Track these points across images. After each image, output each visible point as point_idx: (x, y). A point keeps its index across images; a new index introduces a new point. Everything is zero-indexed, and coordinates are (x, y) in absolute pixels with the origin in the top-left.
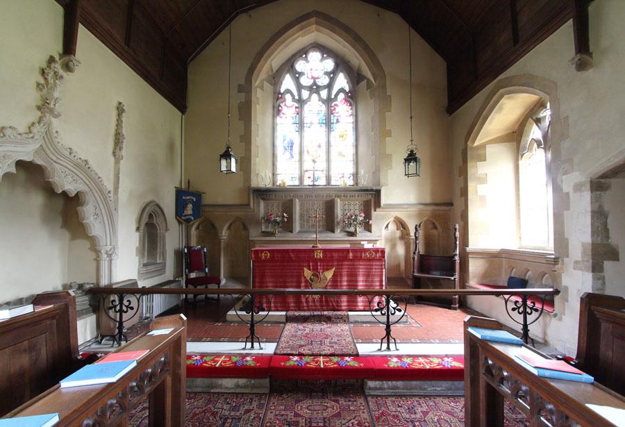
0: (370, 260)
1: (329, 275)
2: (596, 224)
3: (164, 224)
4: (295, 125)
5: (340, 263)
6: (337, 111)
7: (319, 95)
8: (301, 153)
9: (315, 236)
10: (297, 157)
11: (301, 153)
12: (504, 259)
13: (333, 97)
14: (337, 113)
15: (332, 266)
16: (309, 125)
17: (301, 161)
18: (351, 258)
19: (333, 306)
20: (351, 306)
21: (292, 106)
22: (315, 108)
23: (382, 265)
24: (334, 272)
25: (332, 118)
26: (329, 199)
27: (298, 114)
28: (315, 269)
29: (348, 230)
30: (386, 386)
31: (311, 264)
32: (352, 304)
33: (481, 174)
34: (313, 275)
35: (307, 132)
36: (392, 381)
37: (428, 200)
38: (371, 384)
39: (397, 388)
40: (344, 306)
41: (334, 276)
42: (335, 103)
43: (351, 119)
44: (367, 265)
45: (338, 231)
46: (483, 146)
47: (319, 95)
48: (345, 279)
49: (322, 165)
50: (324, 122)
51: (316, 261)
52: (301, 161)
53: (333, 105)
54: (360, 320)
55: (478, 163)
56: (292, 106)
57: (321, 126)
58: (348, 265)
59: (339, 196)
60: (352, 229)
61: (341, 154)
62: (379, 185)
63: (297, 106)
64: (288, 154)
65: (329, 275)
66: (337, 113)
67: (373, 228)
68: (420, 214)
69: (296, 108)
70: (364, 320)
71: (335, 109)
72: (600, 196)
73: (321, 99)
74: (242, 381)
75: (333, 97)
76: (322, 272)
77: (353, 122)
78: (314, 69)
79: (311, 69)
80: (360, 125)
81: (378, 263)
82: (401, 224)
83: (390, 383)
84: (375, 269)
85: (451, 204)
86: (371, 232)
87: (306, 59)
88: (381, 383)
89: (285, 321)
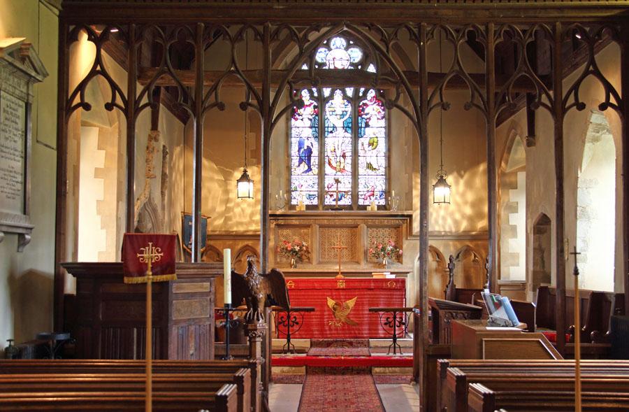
0: (390, 289)
1: (351, 303)
2: (536, 258)
3: (529, 232)
4: (314, 129)
6: (366, 111)
7: (344, 92)
8: (321, 166)
9: (338, 267)
10: (315, 170)
11: (321, 166)
13: (361, 94)
14: (366, 114)
15: (355, 296)
16: (330, 129)
17: (321, 175)
19: (355, 333)
20: (372, 334)
21: (310, 105)
22: (338, 105)
23: (402, 295)
25: (360, 121)
27: (317, 115)
30: (387, 371)
32: (373, 332)
33: (513, 203)
34: (336, 304)
35: (330, 141)
36: (391, 367)
38: (377, 370)
39: (395, 372)
40: (366, 334)
41: (356, 304)
42: (364, 102)
43: (383, 123)
44: (388, 295)
47: (344, 92)
49: (346, 185)
50: (350, 125)
52: (321, 175)
53: (361, 104)
54: (379, 345)
55: (510, 190)
56: (310, 105)
57: (346, 131)
61: (370, 166)
62: (412, 210)
63: (316, 104)
64: (304, 167)
65: (351, 303)
66: (366, 114)
67: (404, 260)
69: (315, 107)
70: (384, 345)
71: (363, 110)
72: (539, 238)
73: (345, 97)
74: (286, 369)
75: (361, 94)
77: (385, 127)
78: (337, 58)
79: (334, 59)
80: (394, 132)
81: (398, 293)
83: (390, 369)
84: (396, 298)
87: (328, 46)
88: (384, 369)
89: (309, 346)
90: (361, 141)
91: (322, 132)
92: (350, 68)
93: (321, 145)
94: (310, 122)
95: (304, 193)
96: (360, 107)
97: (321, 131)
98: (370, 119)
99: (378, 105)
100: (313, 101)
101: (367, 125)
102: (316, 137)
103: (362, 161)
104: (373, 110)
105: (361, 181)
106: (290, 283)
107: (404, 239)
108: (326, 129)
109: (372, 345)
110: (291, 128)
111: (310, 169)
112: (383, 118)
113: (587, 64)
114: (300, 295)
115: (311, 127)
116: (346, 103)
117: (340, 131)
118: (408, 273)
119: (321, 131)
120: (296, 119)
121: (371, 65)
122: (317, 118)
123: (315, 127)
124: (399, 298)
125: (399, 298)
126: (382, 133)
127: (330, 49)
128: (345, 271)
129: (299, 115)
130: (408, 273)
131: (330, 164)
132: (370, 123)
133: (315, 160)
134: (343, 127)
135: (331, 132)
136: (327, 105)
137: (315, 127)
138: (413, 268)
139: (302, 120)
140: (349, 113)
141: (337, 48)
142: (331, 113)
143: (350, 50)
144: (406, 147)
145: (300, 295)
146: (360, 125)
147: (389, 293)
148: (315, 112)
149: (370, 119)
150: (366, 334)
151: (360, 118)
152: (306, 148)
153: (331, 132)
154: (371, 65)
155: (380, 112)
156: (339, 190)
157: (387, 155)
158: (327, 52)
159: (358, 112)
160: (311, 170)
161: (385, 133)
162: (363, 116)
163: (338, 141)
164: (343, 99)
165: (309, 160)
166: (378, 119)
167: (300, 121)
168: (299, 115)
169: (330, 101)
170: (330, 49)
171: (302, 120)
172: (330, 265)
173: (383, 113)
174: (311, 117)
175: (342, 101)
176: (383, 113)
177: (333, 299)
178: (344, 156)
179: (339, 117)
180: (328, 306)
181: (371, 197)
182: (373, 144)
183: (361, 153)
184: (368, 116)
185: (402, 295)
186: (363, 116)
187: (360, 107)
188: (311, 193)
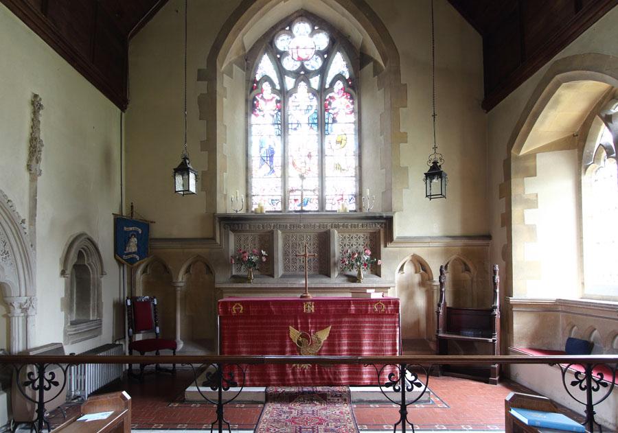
0: (378, 315)
4: (276, 126)
5: (339, 320)
8: (284, 166)
10: (278, 172)
11: (284, 166)
12: (561, 314)
13: (327, 86)
15: (328, 324)
18: (353, 312)
19: (329, 379)
21: (272, 100)
23: (395, 323)
24: (330, 332)
25: (326, 116)
26: (323, 230)
27: (279, 110)
28: (305, 328)
29: (349, 273)
31: (299, 321)
35: (292, 136)
37: (457, 231)
41: (331, 337)
42: (331, 95)
45: (335, 274)
46: (532, 156)
47: (308, 84)
48: (345, 341)
49: (312, 182)
50: (316, 121)
51: (305, 316)
54: (365, 399)
56: (272, 100)
58: (348, 322)
59: (337, 227)
60: (354, 272)
61: (338, 167)
63: (279, 99)
64: (266, 168)
65: (324, 335)
66: (333, 109)
67: (383, 271)
68: (447, 251)
69: (278, 102)
70: (371, 399)
71: (330, 104)
73: (311, 90)
75: (327, 86)
76: (315, 333)
77: (354, 123)
79: (297, 48)
81: (389, 320)
82: (420, 265)
84: (386, 327)
85: (488, 237)
86: (379, 276)
87: (290, 33)
90: (327, 139)
91: (284, 130)
92: (318, 403)
93: (284, 142)
94: (271, 118)
95: (266, 198)
96: (326, 100)
97: (284, 126)
98: (337, 113)
99: (347, 98)
100: (275, 95)
101: (334, 121)
102: (279, 135)
103: (329, 162)
104: (341, 104)
105: (328, 183)
106: (237, 306)
107: (382, 246)
108: (290, 126)
109: (354, 398)
110: (251, 125)
111: (272, 170)
112: (353, 111)
113: (112, 415)
114: (251, 324)
115: (274, 124)
116: (312, 97)
117: (305, 128)
118: (389, 288)
119: (284, 126)
120: (257, 115)
121: (338, 53)
122: (279, 113)
123: (278, 124)
124: (390, 327)
125: (391, 331)
126: (352, 129)
127: (293, 37)
128: (313, 286)
129: (260, 110)
130: (389, 288)
131: (294, 164)
132: (337, 119)
133: (278, 160)
134: (309, 124)
135: (295, 129)
136: (291, 99)
137: (278, 124)
138: (393, 282)
139: (263, 116)
140: (314, 108)
141: (300, 35)
142: (295, 108)
143: (315, 36)
144: (382, 138)
145: (251, 324)
146: (326, 121)
147: (376, 320)
148: (277, 107)
149: (337, 113)
150: (344, 379)
151: (326, 113)
152: (267, 147)
153: (295, 129)
154: (338, 53)
155: (348, 106)
156: (304, 188)
157: (357, 152)
158: (290, 40)
159: (324, 108)
160: (274, 171)
161: (355, 130)
162: (330, 111)
163: (303, 138)
164: (308, 92)
165: (271, 161)
166: (347, 114)
167: (260, 117)
168: (260, 110)
169: (294, 95)
170: (293, 37)
171: (263, 116)
172: (294, 279)
173: (352, 107)
174: (273, 113)
175: (307, 95)
176: (352, 107)
177: (297, 329)
178: (309, 156)
179: (303, 112)
180: (291, 339)
181: (340, 201)
182: (341, 142)
183: (327, 151)
184: (335, 111)
185: (395, 323)
186: (330, 111)
187: (326, 100)
188: (274, 198)
